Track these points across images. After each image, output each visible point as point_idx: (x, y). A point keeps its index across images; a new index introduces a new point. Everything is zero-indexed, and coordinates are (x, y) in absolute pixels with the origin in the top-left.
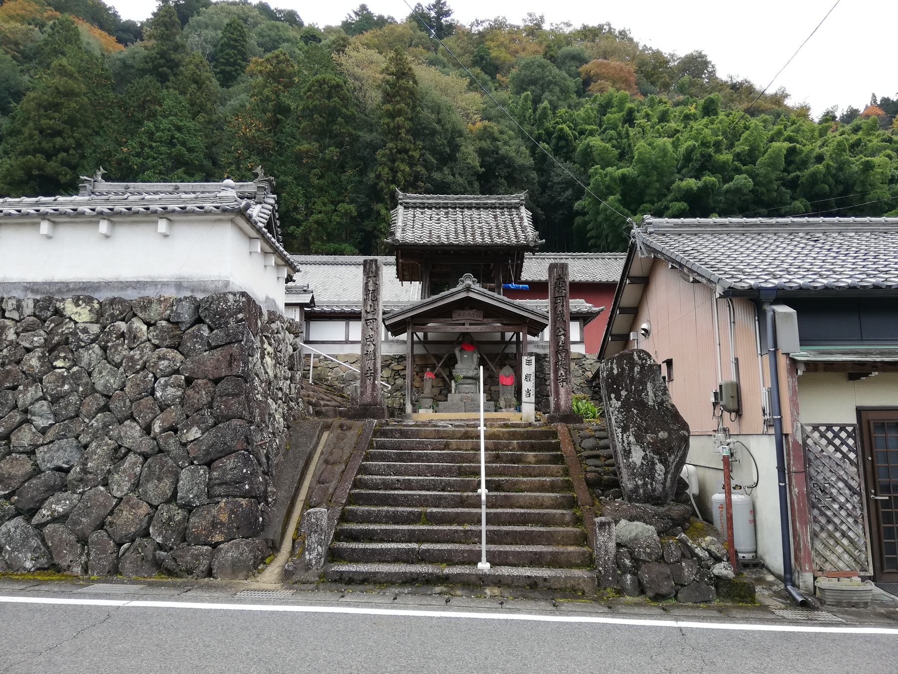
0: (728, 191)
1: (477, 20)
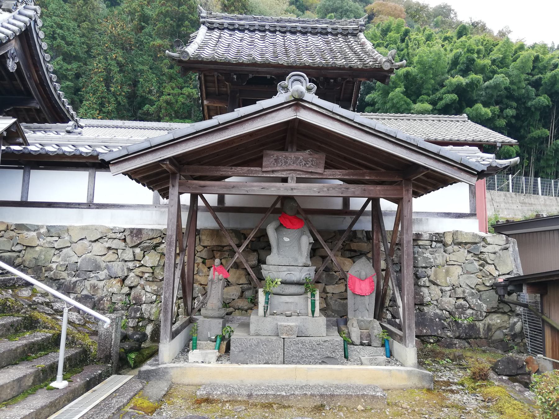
0: (487, 87)
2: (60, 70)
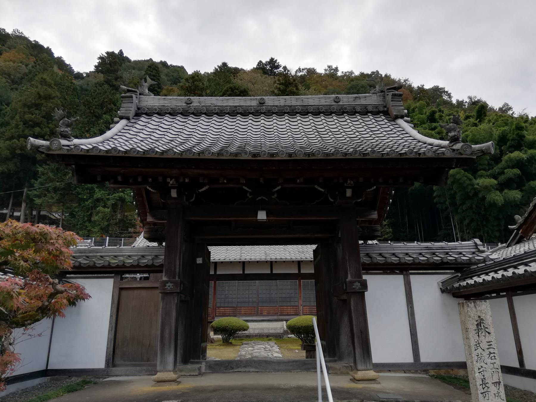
1: (300, 69)
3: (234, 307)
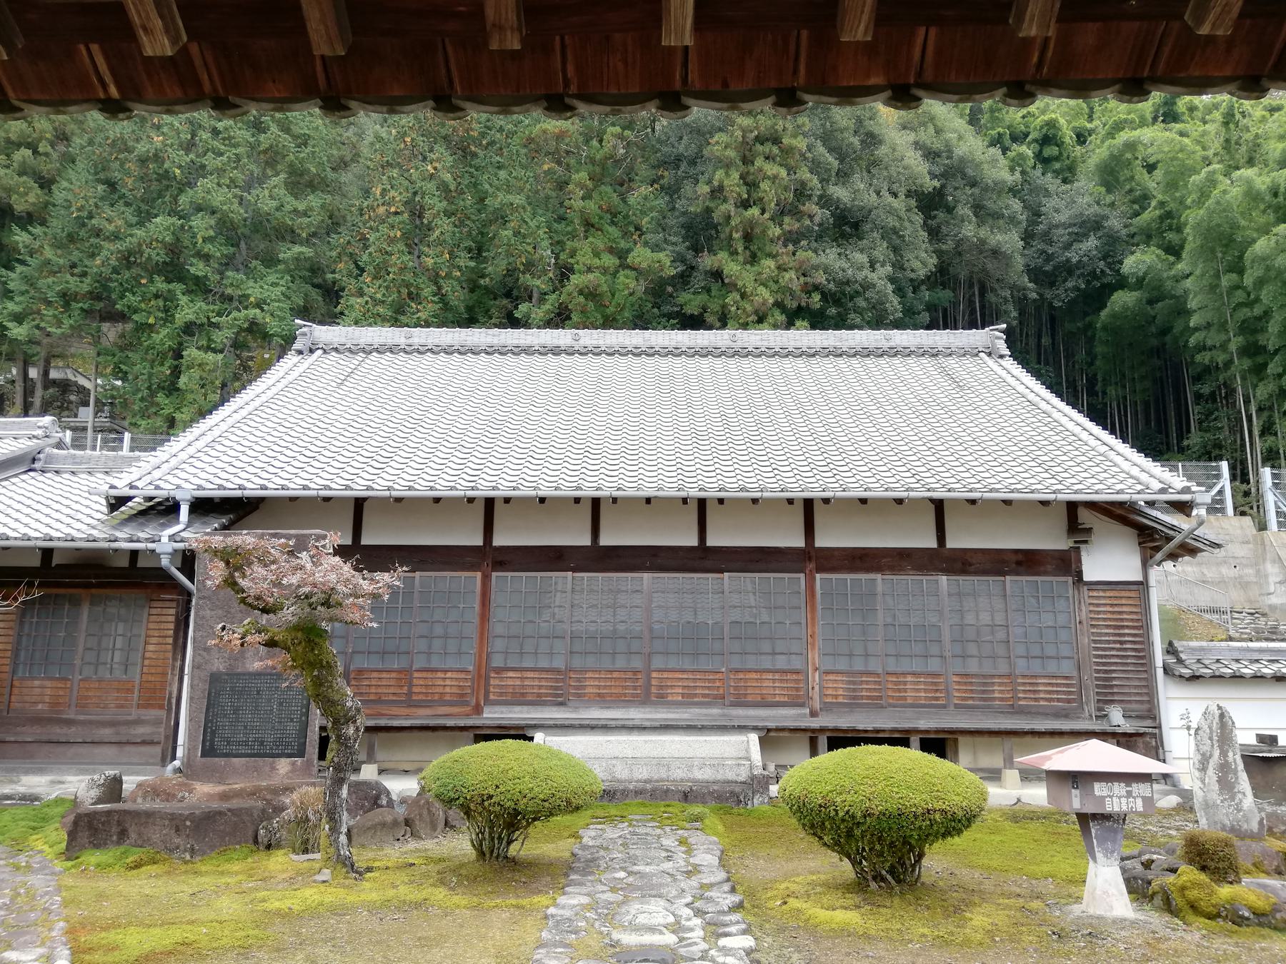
2: (278, 214)
3: (558, 671)
